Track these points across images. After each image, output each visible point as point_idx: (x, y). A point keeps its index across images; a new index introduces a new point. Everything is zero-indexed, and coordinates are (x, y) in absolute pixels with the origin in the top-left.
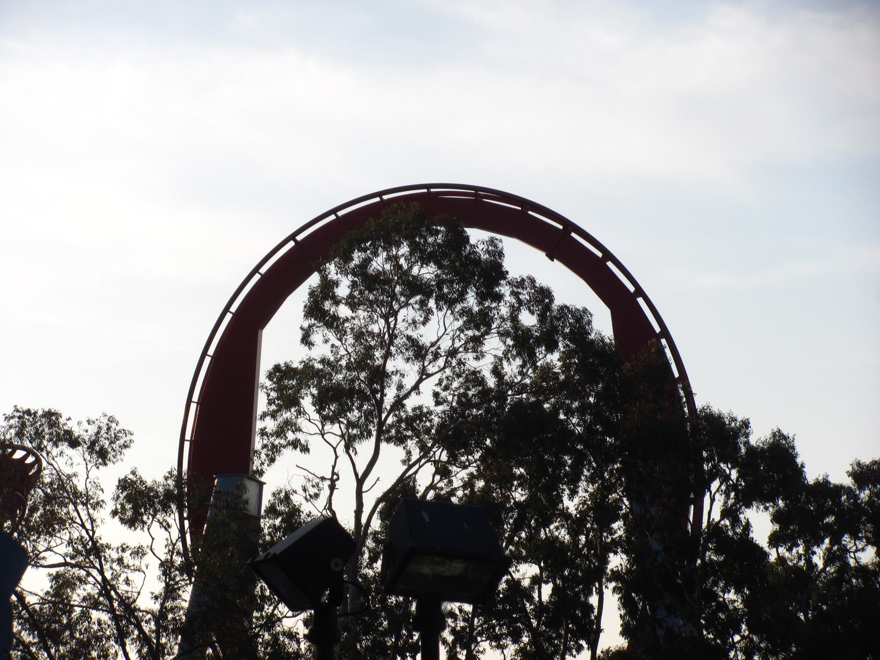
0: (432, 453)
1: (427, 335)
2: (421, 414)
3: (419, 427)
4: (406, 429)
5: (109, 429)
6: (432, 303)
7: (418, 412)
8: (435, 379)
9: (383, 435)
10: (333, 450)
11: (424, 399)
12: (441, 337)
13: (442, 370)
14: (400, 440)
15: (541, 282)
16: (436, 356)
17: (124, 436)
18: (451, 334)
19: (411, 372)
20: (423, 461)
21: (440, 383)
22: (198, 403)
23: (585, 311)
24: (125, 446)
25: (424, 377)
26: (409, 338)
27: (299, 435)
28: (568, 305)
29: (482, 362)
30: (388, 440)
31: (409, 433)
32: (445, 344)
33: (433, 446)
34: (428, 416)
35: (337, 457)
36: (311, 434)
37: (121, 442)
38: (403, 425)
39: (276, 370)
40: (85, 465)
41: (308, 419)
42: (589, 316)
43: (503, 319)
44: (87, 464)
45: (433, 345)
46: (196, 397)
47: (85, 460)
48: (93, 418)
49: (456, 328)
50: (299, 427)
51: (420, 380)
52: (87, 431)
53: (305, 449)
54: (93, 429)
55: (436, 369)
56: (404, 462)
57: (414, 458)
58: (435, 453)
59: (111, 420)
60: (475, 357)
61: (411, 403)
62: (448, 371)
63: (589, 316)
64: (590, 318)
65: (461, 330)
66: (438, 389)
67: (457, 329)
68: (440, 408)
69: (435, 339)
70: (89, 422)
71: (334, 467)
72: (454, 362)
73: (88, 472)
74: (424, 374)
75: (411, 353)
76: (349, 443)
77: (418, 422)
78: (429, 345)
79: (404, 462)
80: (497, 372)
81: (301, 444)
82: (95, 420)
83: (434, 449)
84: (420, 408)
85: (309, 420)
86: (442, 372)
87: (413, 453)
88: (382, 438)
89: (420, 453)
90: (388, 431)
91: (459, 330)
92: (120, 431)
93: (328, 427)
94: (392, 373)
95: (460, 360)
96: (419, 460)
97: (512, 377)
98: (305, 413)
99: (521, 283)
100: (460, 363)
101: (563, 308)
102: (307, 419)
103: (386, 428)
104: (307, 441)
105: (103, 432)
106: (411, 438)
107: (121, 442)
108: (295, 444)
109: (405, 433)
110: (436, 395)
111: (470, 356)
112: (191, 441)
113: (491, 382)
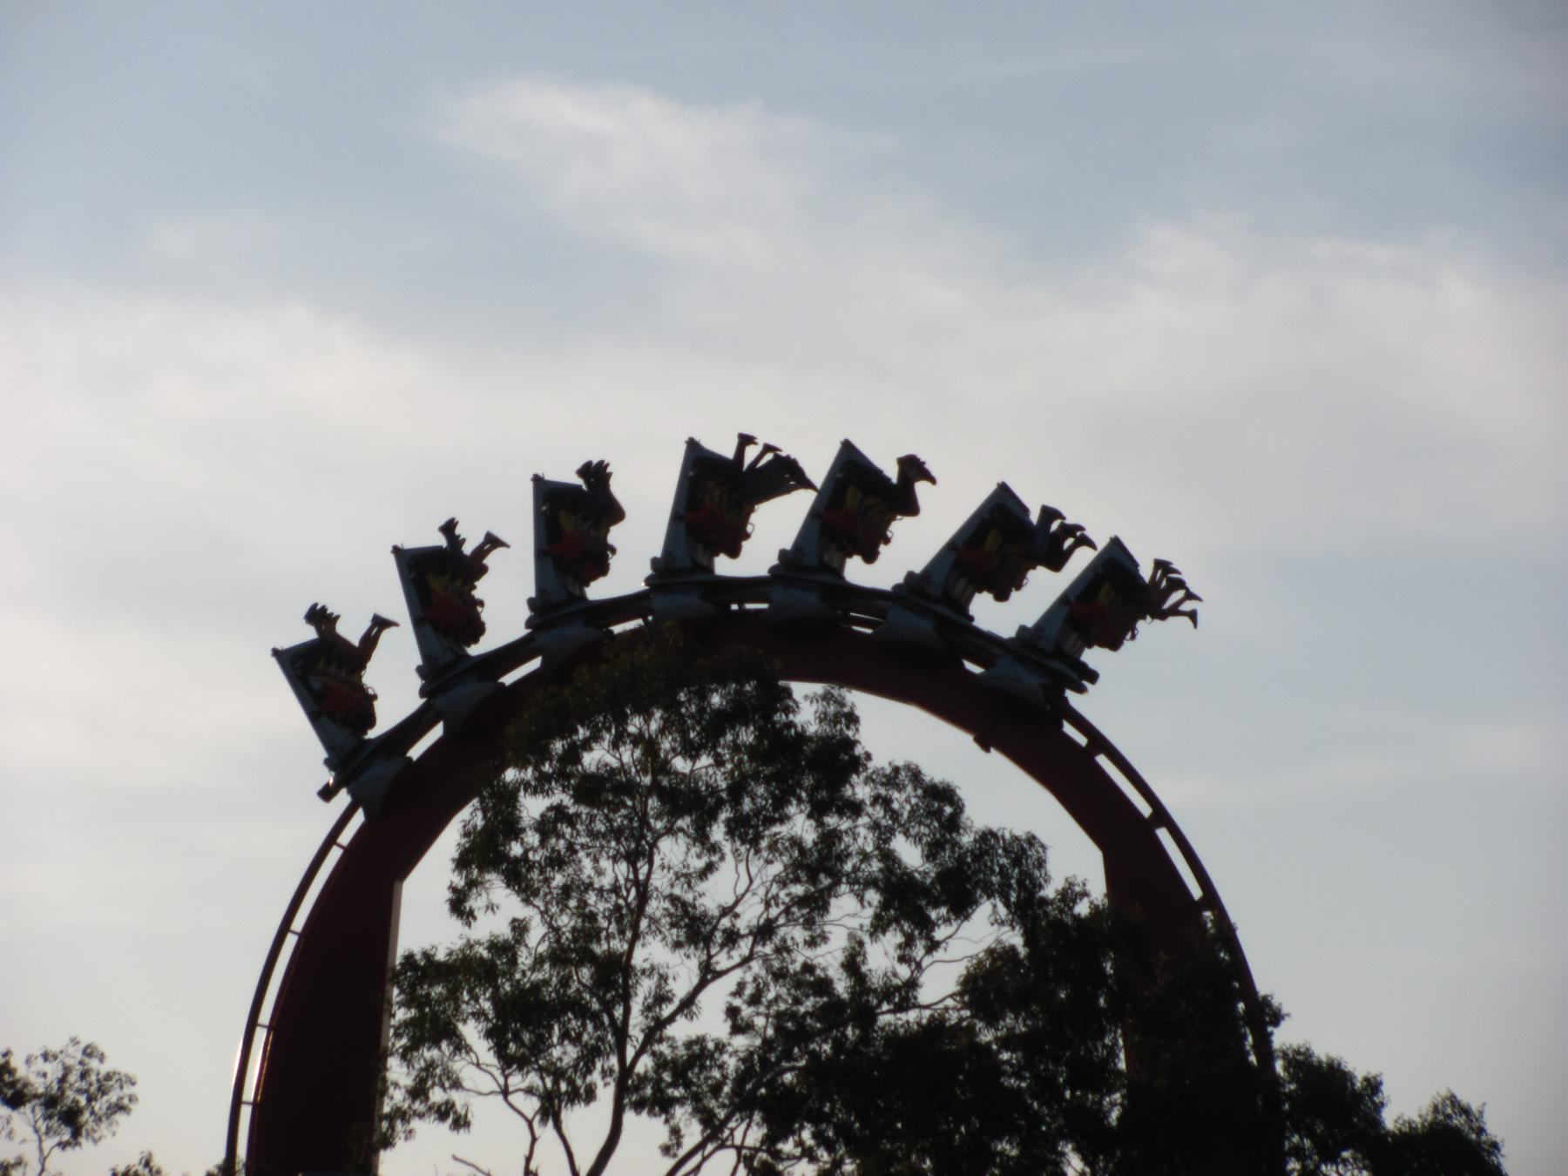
0: (727, 1133)
1: (714, 894)
2: (700, 1054)
3: (699, 1078)
4: (674, 1085)
5: (84, 1075)
6: (718, 833)
7: (696, 1048)
8: (728, 983)
9: (630, 1094)
10: (524, 1124)
11: (709, 1021)
12: (743, 895)
13: (746, 961)
14: (661, 1105)
15: (934, 773)
16: (732, 938)
17: (117, 1085)
18: (762, 892)
19: (683, 971)
20: (710, 1147)
21: (739, 992)
22: (270, 1028)
23: (1032, 840)
24: (119, 1108)
25: (709, 977)
26: (673, 899)
27: (457, 1097)
28: (995, 830)
29: (823, 949)
30: (638, 1106)
31: (677, 1093)
32: (751, 914)
33: (728, 1118)
34: (716, 1055)
35: (534, 1140)
36: (480, 1094)
37: (113, 1097)
38: (667, 1077)
39: (407, 968)
40: (38, 1143)
41: (475, 1061)
42: (1040, 850)
43: (866, 857)
44: (40, 1141)
45: (727, 911)
46: (265, 1016)
47: (36, 1131)
48: (54, 1047)
49: (770, 878)
50: (458, 1079)
51: (702, 984)
52: (45, 1075)
53: (461, 1123)
54: (53, 1070)
55: (737, 960)
56: (666, 1150)
57: (690, 1141)
58: (732, 1130)
59: (89, 1052)
60: (807, 938)
61: (681, 1031)
62: (756, 966)
63: (1040, 850)
64: (1043, 854)
65: (782, 882)
66: (737, 1002)
67: (773, 880)
68: (741, 1042)
69: (730, 901)
70: (46, 1057)
71: (528, 1159)
72: (768, 949)
73: (45, 1159)
74: (708, 974)
75: (681, 934)
76: (550, 1110)
77: (696, 1070)
78: (716, 913)
79: (666, 1150)
80: (852, 965)
81: (455, 1112)
82: (59, 1054)
83: (732, 1124)
84: (700, 1041)
85: (478, 1065)
86: (745, 968)
87: (684, 1131)
88: (626, 1101)
89: (703, 1132)
90: (637, 1088)
91: (779, 882)
92: (108, 1077)
93: (516, 1080)
94: (643, 972)
95: (784, 940)
96: (700, 1146)
97: (888, 978)
98: (469, 1050)
99: (892, 779)
100: (783, 949)
101: (987, 837)
102: (473, 1064)
103: (633, 1082)
104: (467, 1106)
105: (73, 1078)
106: (680, 1101)
107: (113, 1097)
108: (444, 1112)
109: (670, 1091)
110: (732, 1012)
111: (799, 934)
112: (255, 1105)
113: (842, 986)
